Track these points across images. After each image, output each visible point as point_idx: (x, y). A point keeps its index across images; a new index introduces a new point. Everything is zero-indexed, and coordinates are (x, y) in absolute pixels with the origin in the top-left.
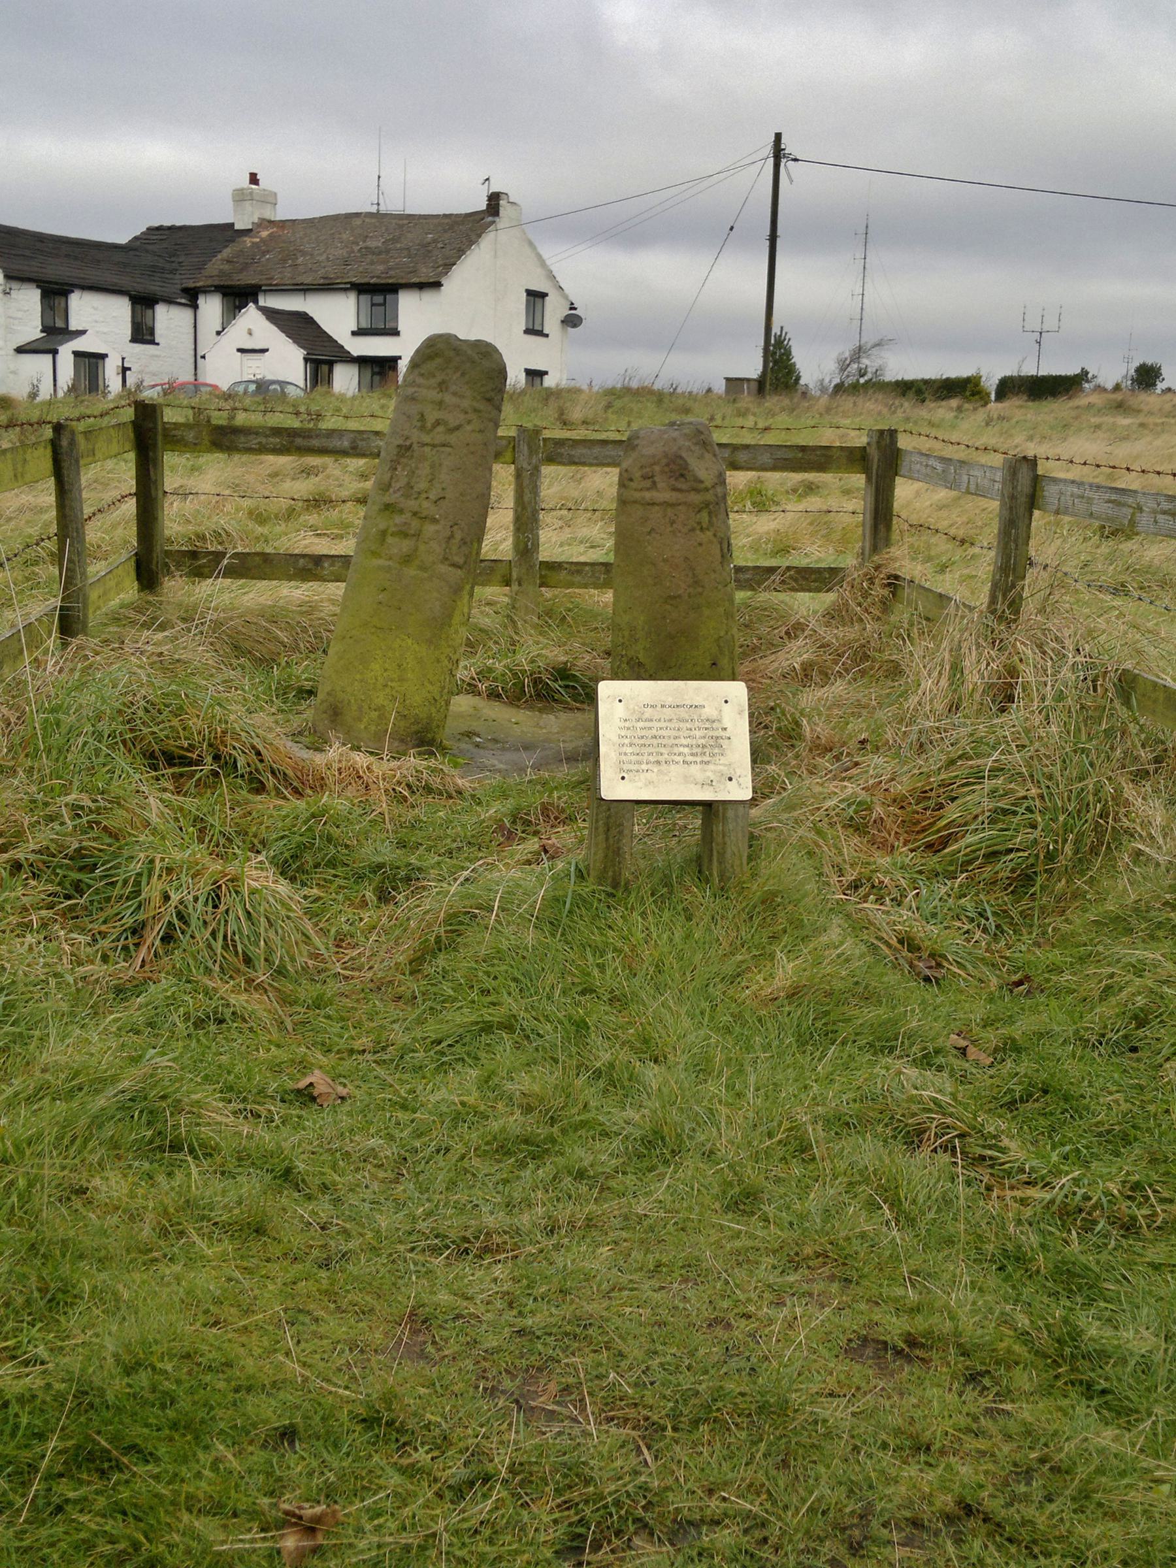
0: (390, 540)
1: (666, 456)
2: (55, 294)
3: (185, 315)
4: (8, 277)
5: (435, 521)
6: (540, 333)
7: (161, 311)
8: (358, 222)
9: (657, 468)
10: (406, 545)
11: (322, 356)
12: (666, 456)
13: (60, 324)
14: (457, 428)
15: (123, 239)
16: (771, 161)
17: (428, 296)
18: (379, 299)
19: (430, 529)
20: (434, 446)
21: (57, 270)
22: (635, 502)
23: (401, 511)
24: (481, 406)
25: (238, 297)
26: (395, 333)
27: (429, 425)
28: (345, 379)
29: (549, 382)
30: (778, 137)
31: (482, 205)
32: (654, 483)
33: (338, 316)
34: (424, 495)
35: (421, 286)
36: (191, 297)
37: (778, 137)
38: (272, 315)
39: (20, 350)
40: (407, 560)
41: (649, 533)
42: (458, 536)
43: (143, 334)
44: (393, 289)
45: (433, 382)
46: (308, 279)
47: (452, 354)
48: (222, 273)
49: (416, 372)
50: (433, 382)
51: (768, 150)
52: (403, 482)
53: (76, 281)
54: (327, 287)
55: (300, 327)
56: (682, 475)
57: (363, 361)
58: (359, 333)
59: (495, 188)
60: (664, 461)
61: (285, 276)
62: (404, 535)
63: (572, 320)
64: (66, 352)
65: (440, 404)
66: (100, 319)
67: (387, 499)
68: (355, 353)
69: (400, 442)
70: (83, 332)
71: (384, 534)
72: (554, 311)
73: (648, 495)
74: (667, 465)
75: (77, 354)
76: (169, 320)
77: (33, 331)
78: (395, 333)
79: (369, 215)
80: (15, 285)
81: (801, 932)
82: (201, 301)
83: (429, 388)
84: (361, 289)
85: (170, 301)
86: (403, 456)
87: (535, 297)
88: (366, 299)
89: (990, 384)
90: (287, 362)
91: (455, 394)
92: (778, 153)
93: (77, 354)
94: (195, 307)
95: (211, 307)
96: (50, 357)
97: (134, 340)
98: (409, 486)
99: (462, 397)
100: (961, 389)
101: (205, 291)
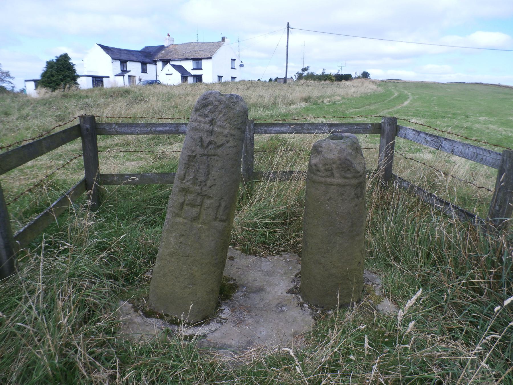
0: (185, 207)
1: (340, 159)
2: (123, 62)
4: (113, 59)
5: (210, 197)
6: (234, 69)
7: (148, 65)
8: (192, 44)
9: (334, 165)
10: (194, 211)
11: (185, 75)
12: (340, 159)
13: (125, 69)
14: (222, 145)
16: (287, 29)
17: (209, 60)
18: (197, 62)
19: (208, 202)
20: (208, 156)
21: (123, 57)
22: (322, 183)
23: (191, 193)
24: (235, 132)
25: (166, 62)
26: (202, 69)
27: (205, 145)
28: (190, 80)
29: (237, 80)
30: (288, 23)
31: (221, 40)
32: (332, 174)
33: (188, 66)
34: (204, 184)
35: (207, 58)
37: (288, 23)
38: (173, 66)
39: (116, 76)
40: (195, 219)
41: (328, 200)
42: (223, 204)
43: (144, 71)
44: (201, 59)
45: (207, 120)
46: (181, 57)
47: (218, 103)
48: (161, 57)
49: (198, 113)
50: (207, 120)
51: (286, 26)
52: (191, 177)
53: (202, 56)
55: (179, 68)
56: (349, 170)
57: (194, 76)
59: (223, 36)
60: (339, 162)
61: (176, 57)
62: (192, 205)
63: (242, 66)
64: (126, 75)
65: (211, 132)
67: (183, 185)
69: (190, 153)
70: (130, 71)
71: (182, 204)
72: (237, 64)
73: (328, 180)
74: (340, 164)
75: (129, 76)
76: (150, 67)
77: (119, 71)
78: (202, 69)
79: (195, 43)
80: (114, 61)
82: (157, 63)
83: (205, 123)
84: (193, 59)
85: (150, 63)
86: (192, 161)
87: (233, 60)
88: (194, 62)
90: (176, 78)
91: (220, 126)
92: (288, 27)
93: (129, 76)
94: (156, 64)
95: (160, 64)
97: (142, 72)
98: (195, 178)
99: (224, 128)
101: (158, 61)
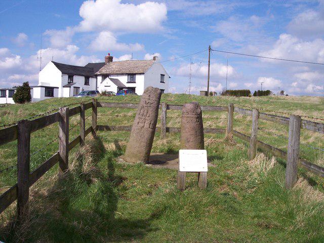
2: (71, 77)
3: (95, 79)
15: (149, 3)
21: (71, 71)
36: (96, 76)
38: (111, 79)
43: (87, 83)
46: (118, 72)
51: (208, 49)
54: (122, 74)
55: (116, 82)
58: (128, 82)
64: (72, 87)
66: (79, 81)
68: (127, 86)
77: (66, 83)
78: (135, 82)
81: (286, 143)
82: (98, 77)
84: (128, 74)
87: (162, 75)
89: (252, 92)
92: (210, 49)
96: (69, 88)
100: (246, 93)
101: (99, 75)
